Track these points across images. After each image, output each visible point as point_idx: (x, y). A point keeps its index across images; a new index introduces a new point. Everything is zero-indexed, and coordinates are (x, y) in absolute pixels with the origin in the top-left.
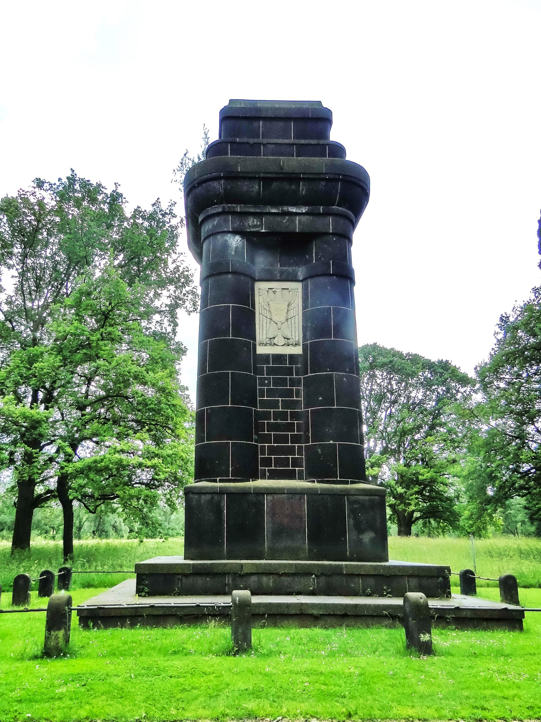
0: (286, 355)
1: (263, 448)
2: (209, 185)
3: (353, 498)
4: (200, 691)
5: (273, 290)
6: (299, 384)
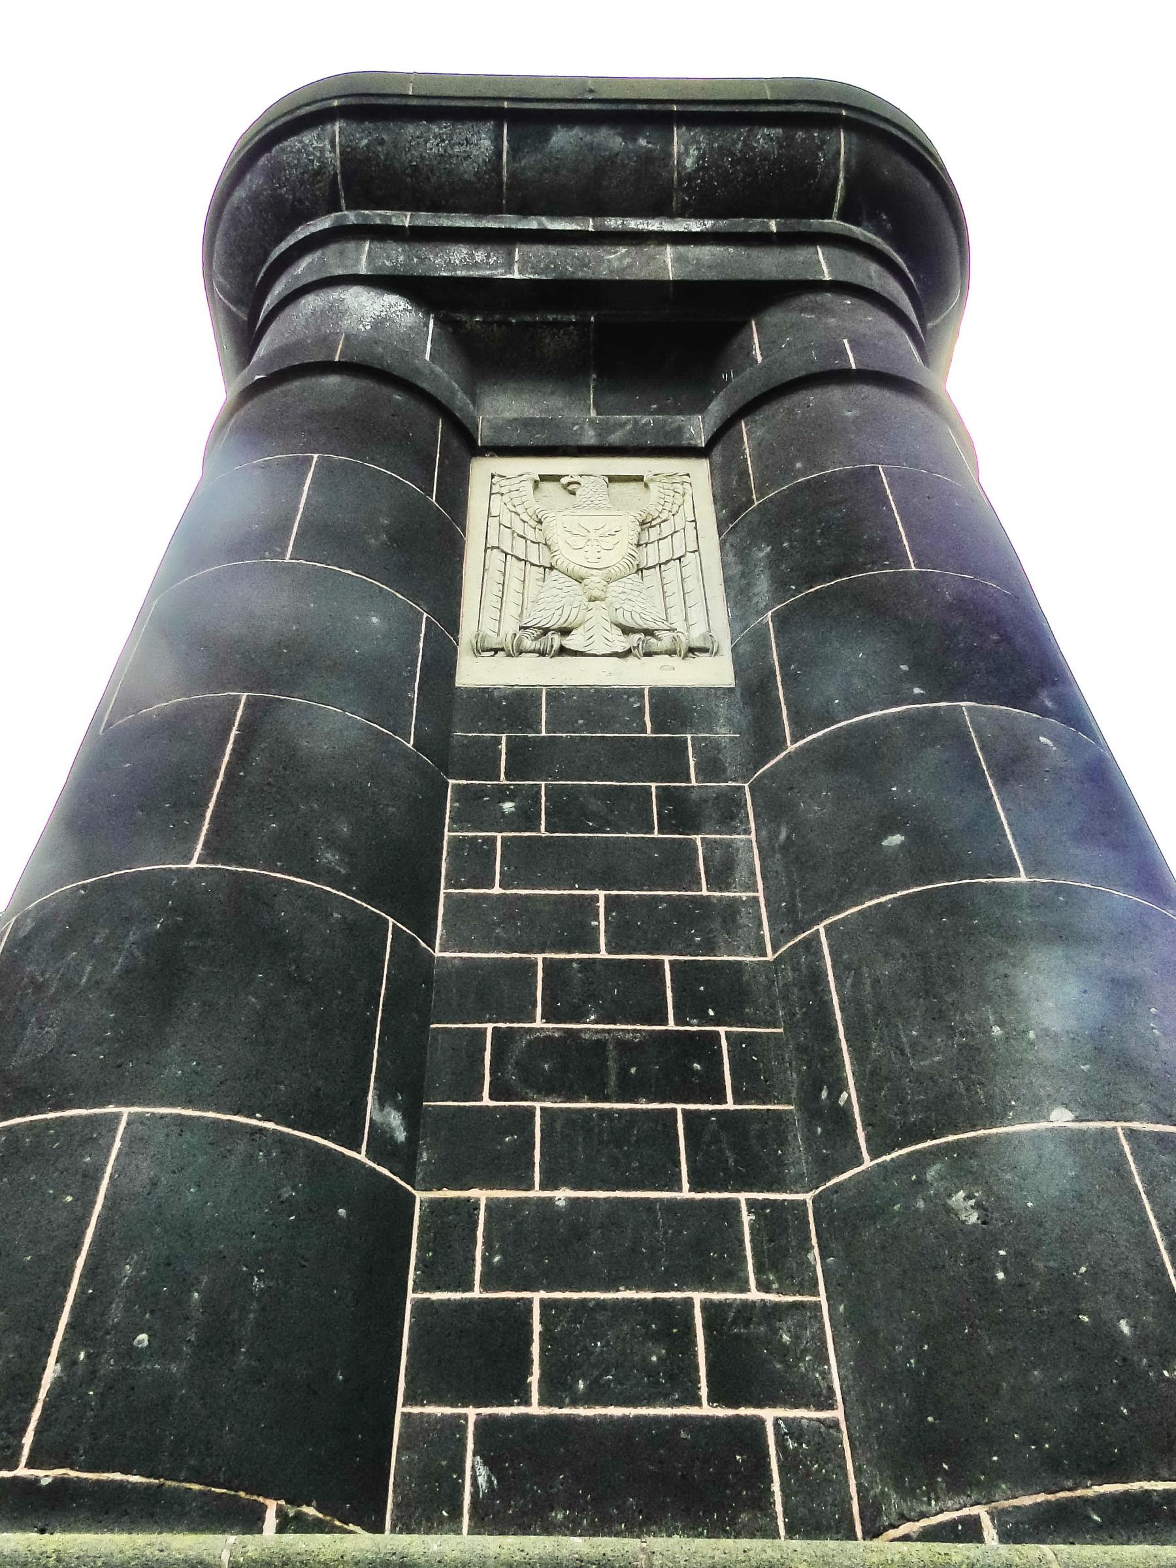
0: (639, 693)
1: (452, 1223)
2: (283, 150)
5: (564, 481)
6: (728, 812)
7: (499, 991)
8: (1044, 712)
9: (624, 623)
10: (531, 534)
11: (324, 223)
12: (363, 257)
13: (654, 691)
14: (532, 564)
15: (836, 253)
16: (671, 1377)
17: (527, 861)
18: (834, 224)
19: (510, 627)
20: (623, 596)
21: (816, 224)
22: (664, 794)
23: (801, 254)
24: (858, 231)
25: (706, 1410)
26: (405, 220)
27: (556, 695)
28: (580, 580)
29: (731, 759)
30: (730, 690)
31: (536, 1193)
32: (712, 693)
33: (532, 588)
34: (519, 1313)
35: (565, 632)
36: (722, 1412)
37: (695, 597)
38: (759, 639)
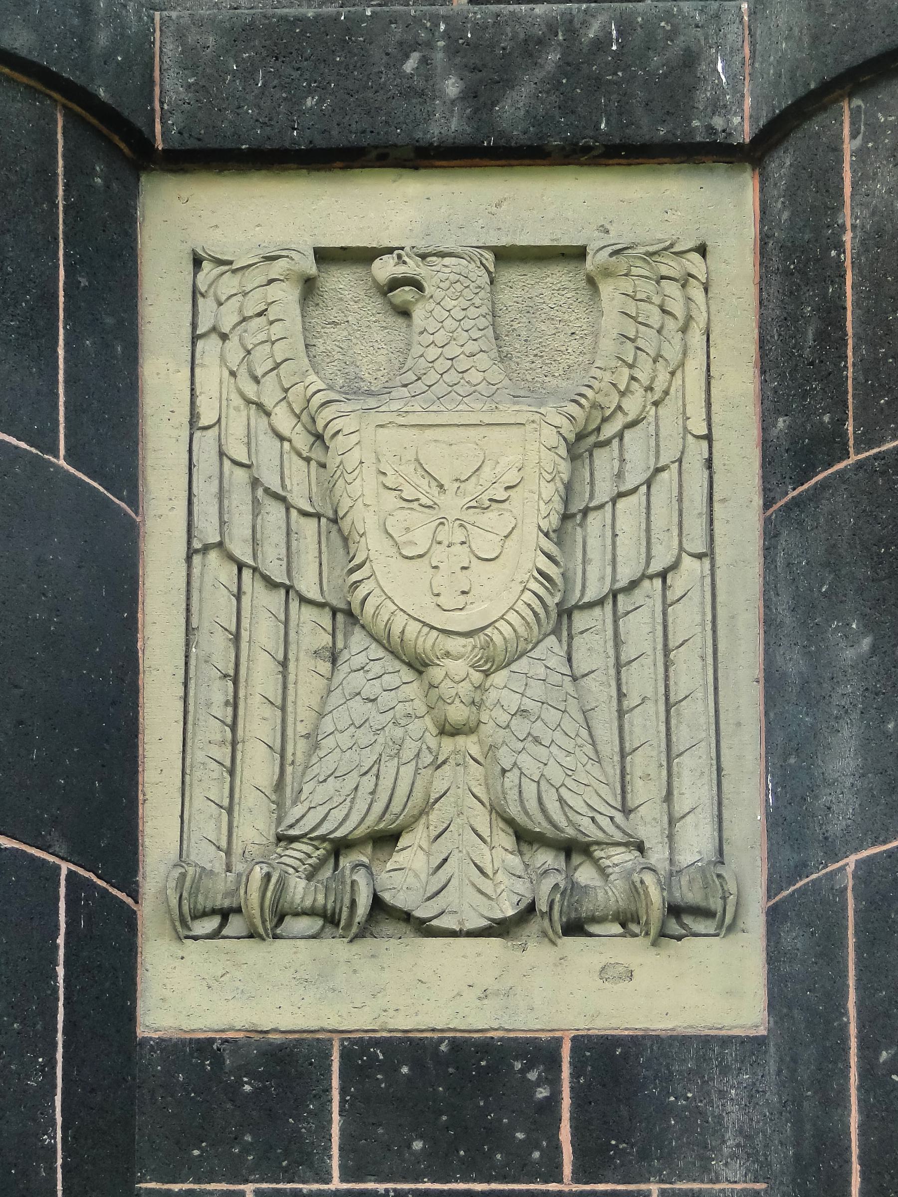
9: (521, 819)
13: (581, 1043)
14: (303, 600)
20: (521, 727)
27: (370, 1057)
28: (418, 665)
30: (759, 1042)
37: (694, 716)
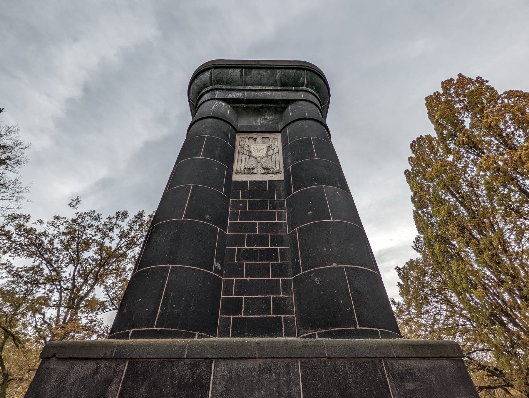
0: (266, 182)
3: (399, 365)
4: (508, 229)
6: (282, 206)
7: (239, 241)
8: (338, 187)
10: (247, 149)
11: (209, 88)
12: (217, 94)
15: (304, 93)
16: (266, 310)
17: (245, 215)
18: (304, 88)
19: (243, 168)
21: (300, 88)
22: (270, 202)
23: (299, 93)
24: (310, 90)
25: (272, 316)
26: (225, 87)
27: (251, 182)
28: (256, 158)
29: (283, 194)
31: (244, 278)
32: (279, 181)
33: (247, 160)
34: (240, 300)
35: (253, 169)
36: (274, 316)
38: (289, 170)
